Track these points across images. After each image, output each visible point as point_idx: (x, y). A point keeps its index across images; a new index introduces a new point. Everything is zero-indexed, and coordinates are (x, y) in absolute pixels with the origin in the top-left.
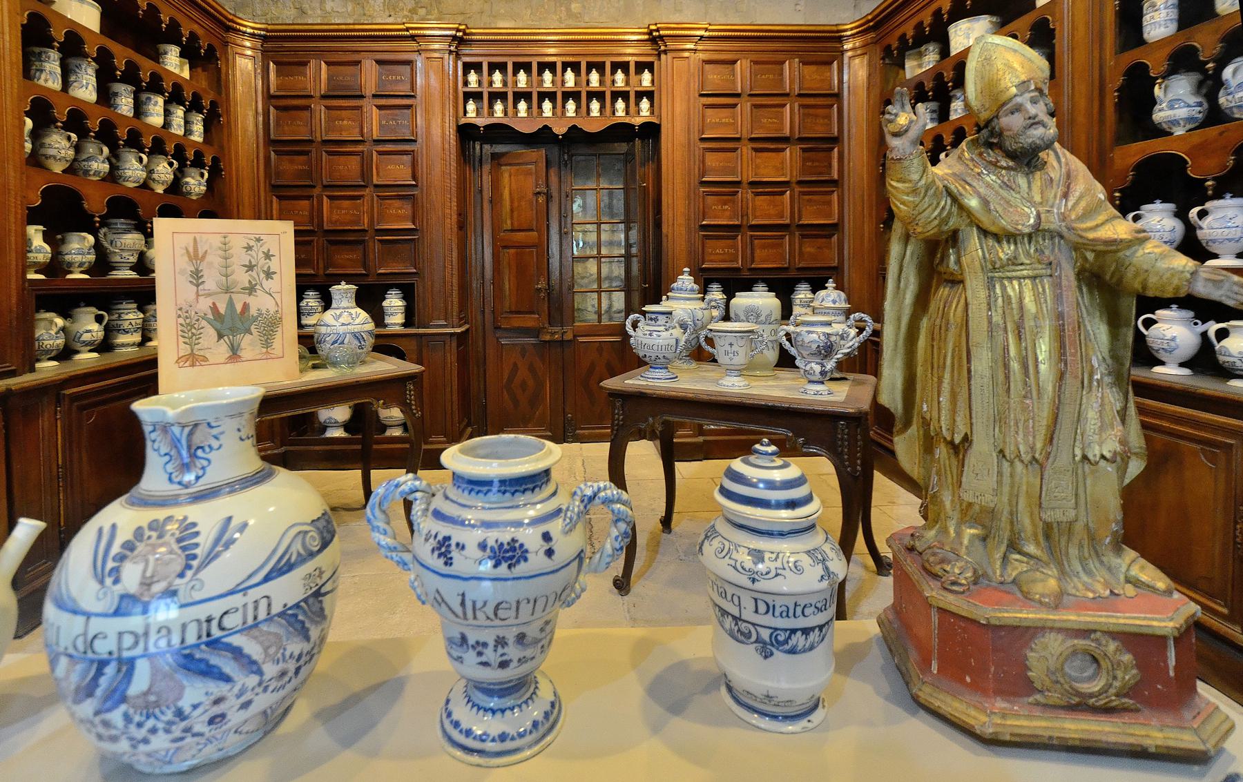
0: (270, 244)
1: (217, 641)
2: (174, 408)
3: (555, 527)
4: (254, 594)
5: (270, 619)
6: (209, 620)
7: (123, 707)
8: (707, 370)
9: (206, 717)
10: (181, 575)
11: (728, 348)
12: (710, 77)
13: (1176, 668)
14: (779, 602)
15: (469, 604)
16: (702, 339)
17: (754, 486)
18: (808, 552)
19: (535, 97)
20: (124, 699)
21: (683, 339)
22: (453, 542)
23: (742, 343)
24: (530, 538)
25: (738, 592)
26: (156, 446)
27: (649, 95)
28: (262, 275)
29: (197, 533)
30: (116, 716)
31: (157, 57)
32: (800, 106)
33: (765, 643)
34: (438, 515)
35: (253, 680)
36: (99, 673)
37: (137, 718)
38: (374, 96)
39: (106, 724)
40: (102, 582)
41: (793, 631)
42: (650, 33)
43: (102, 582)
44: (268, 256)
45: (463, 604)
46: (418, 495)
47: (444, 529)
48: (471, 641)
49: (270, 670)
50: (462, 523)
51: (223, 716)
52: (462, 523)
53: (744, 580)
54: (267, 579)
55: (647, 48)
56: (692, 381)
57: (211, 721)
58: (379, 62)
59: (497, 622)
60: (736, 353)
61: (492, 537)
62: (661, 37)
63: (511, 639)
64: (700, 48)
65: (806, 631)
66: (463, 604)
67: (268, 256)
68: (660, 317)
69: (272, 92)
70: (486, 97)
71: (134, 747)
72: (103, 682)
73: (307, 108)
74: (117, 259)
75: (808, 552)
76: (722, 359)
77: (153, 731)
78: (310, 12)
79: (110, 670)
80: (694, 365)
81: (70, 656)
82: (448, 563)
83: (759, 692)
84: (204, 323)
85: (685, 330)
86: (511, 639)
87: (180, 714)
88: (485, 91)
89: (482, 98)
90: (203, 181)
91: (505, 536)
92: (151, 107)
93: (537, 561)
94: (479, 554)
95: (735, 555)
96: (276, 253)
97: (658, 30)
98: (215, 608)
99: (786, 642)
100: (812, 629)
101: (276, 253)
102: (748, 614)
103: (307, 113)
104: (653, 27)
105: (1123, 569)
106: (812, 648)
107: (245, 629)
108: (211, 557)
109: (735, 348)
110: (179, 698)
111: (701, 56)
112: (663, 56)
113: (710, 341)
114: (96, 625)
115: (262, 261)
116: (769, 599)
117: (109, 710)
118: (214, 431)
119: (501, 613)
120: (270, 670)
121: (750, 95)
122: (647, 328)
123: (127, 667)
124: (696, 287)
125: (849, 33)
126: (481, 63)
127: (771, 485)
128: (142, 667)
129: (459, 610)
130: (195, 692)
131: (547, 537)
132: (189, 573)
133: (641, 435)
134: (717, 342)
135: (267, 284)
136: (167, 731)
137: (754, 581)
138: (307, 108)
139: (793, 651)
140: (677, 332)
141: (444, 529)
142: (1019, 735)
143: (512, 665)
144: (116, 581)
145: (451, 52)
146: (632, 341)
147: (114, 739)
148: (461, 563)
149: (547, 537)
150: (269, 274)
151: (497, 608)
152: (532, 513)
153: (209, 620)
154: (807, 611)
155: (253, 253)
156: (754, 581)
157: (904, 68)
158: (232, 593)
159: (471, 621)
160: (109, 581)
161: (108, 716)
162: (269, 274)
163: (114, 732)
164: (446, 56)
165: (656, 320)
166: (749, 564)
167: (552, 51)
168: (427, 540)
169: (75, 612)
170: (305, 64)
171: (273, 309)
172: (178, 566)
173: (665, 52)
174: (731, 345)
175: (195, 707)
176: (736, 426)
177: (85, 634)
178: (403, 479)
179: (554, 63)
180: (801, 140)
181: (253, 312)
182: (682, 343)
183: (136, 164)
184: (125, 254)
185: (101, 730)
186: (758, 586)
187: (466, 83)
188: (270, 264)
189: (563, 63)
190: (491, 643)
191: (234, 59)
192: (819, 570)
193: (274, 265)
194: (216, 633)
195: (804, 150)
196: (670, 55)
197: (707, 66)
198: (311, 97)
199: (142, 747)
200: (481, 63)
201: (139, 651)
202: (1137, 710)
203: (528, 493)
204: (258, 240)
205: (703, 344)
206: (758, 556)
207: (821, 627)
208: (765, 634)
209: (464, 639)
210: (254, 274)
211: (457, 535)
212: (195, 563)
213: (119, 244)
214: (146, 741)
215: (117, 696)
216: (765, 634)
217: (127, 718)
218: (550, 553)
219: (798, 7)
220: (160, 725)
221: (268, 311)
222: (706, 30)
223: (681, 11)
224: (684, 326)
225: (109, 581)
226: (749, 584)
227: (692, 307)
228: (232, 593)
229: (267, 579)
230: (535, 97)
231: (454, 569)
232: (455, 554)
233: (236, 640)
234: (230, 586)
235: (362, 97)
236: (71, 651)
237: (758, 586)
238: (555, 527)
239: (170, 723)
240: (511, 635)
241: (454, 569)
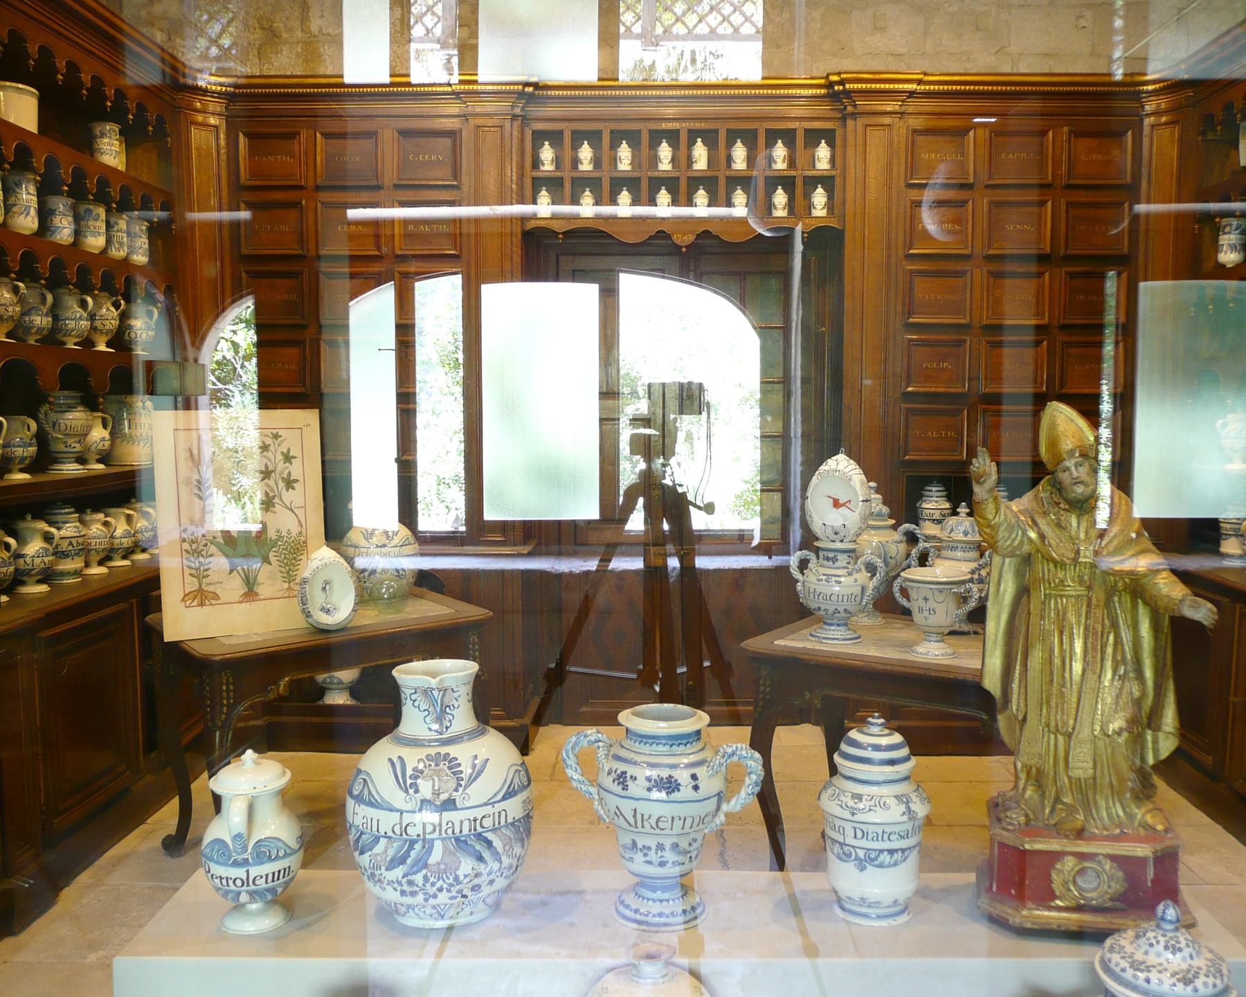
0: (290, 442)
1: (480, 834)
2: (434, 678)
3: (701, 772)
4: (499, 807)
5: (507, 826)
6: (475, 820)
7: (424, 871)
8: (899, 632)
9: (470, 886)
10: (456, 790)
11: (921, 603)
12: (925, 156)
13: (1152, 881)
14: (871, 829)
15: (639, 817)
16: (896, 589)
17: (865, 749)
18: (896, 797)
19: (645, 185)
20: (426, 866)
21: (871, 585)
22: (628, 775)
23: (940, 598)
24: (683, 776)
25: (843, 823)
26: (416, 704)
27: (826, 181)
28: (281, 485)
29: (459, 765)
30: (418, 878)
31: (88, 146)
32: (1068, 204)
33: (860, 860)
34: (617, 758)
35: (496, 866)
36: (411, 848)
37: (432, 880)
38: (396, 186)
39: (410, 883)
40: (407, 792)
41: (881, 851)
42: (830, 85)
43: (407, 792)
44: (288, 458)
45: (635, 816)
46: (601, 744)
47: (622, 767)
48: (640, 846)
49: (506, 861)
50: (635, 763)
51: (479, 886)
52: (635, 763)
53: (847, 815)
54: (504, 799)
55: (824, 109)
56: (876, 646)
57: (473, 889)
58: (404, 133)
59: (658, 831)
60: (932, 611)
61: (653, 773)
62: (848, 93)
63: (668, 847)
64: (910, 109)
65: (891, 852)
66: (635, 816)
67: (288, 458)
68: (840, 557)
69: (243, 180)
70: (567, 185)
71: (426, 900)
72: (413, 854)
73: (296, 204)
74: (61, 447)
75: (896, 797)
76: (917, 617)
77: (440, 890)
78: (285, 35)
79: (418, 846)
80: (879, 620)
81: (390, 838)
82: (625, 788)
83: (856, 896)
84: (213, 549)
85: (873, 575)
86: (668, 847)
87: (456, 879)
88: (567, 175)
89: (562, 185)
90: (152, 323)
91: (665, 773)
92: (91, 223)
93: (686, 792)
94: (647, 784)
95: (842, 798)
96: (298, 454)
97: (842, 82)
98: (479, 813)
99: (876, 859)
100: (896, 851)
101: (298, 454)
102: (850, 840)
103: (294, 214)
104: (834, 78)
105: (1139, 817)
106: (895, 864)
107: (494, 830)
108: (473, 779)
109: (931, 604)
110: (457, 869)
111: (916, 122)
112: (850, 123)
113: (904, 592)
114: (407, 818)
115: (281, 465)
116: (864, 827)
117: (415, 873)
118: (456, 695)
119: (661, 825)
120: (506, 861)
121: (988, 186)
122: (822, 570)
123: (428, 846)
124: (885, 510)
125: (1150, 88)
126: (561, 132)
127: (877, 748)
128: (438, 846)
129: (632, 821)
130: (466, 866)
131: (694, 777)
132: (461, 789)
133: (796, 717)
134: (913, 594)
135: (288, 496)
136: (449, 891)
137: (853, 814)
138: (296, 204)
139: (881, 866)
140: (863, 576)
141: (622, 767)
142: (1038, 924)
143: (669, 865)
144: (417, 791)
145: (514, 117)
146: (799, 587)
147: (413, 894)
148: (635, 789)
149: (694, 777)
150: (290, 483)
151: (657, 822)
152: (686, 761)
153: (475, 820)
154: (892, 837)
155: (270, 455)
156: (853, 814)
157: (1237, 148)
158: (486, 804)
159: (640, 829)
160: (411, 791)
161: (412, 877)
162: (290, 483)
163: (415, 888)
164: (508, 125)
165: (834, 560)
166: (851, 803)
167: (670, 111)
168: (609, 774)
169: (391, 810)
170: (292, 136)
171: (295, 530)
172: (453, 784)
173: (854, 116)
174: (926, 599)
175: (466, 876)
176: (930, 707)
177: (401, 824)
178: (589, 732)
179: (677, 132)
180: (1069, 258)
181: (272, 534)
182: (869, 592)
183: (79, 312)
184: (70, 441)
185: (406, 888)
186: (856, 818)
187: (536, 163)
188: (291, 468)
189: (690, 131)
190: (654, 847)
191: (189, 132)
192: (903, 808)
193: (295, 470)
194: (479, 829)
195: (1073, 275)
196: (861, 121)
197: (921, 138)
198: (300, 188)
199: (432, 901)
200: (561, 132)
201: (436, 835)
202: (1125, 910)
203: (682, 747)
204: (276, 436)
205: (897, 595)
206: (858, 797)
207: (903, 851)
208: (861, 853)
209: (634, 844)
210: (271, 482)
211: (631, 770)
212: (463, 783)
213: (63, 427)
214: (435, 896)
215: (422, 863)
216: (861, 853)
217: (426, 878)
218: (696, 788)
219: (1083, 22)
220: (445, 886)
221: (289, 532)
222: (920, 82)
223: (882, 29)
224: (871, 569)
225: (411, 791)
226: (849, 817)
227: (883, 540)
228: (486, 804)
229: (504, 799)
230: (645, 185)
231: (630, 792)
232: (629, 783)
233: (490, 836)
234: (481, 802)
235: (378, 188)
236: (390, 834)
237: (856, 818)
238: (701, 772)
239: (451, 885)
240: (668, 843)
241: (630, 792)
